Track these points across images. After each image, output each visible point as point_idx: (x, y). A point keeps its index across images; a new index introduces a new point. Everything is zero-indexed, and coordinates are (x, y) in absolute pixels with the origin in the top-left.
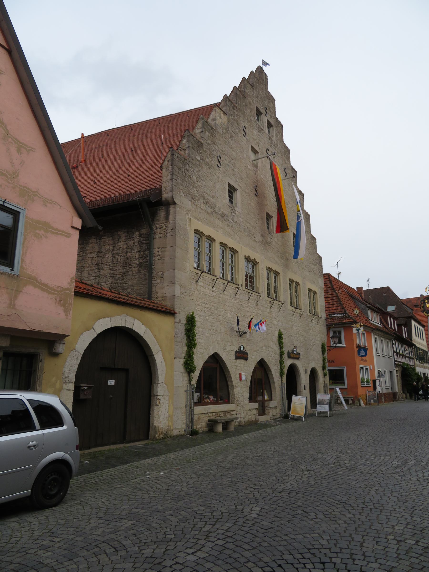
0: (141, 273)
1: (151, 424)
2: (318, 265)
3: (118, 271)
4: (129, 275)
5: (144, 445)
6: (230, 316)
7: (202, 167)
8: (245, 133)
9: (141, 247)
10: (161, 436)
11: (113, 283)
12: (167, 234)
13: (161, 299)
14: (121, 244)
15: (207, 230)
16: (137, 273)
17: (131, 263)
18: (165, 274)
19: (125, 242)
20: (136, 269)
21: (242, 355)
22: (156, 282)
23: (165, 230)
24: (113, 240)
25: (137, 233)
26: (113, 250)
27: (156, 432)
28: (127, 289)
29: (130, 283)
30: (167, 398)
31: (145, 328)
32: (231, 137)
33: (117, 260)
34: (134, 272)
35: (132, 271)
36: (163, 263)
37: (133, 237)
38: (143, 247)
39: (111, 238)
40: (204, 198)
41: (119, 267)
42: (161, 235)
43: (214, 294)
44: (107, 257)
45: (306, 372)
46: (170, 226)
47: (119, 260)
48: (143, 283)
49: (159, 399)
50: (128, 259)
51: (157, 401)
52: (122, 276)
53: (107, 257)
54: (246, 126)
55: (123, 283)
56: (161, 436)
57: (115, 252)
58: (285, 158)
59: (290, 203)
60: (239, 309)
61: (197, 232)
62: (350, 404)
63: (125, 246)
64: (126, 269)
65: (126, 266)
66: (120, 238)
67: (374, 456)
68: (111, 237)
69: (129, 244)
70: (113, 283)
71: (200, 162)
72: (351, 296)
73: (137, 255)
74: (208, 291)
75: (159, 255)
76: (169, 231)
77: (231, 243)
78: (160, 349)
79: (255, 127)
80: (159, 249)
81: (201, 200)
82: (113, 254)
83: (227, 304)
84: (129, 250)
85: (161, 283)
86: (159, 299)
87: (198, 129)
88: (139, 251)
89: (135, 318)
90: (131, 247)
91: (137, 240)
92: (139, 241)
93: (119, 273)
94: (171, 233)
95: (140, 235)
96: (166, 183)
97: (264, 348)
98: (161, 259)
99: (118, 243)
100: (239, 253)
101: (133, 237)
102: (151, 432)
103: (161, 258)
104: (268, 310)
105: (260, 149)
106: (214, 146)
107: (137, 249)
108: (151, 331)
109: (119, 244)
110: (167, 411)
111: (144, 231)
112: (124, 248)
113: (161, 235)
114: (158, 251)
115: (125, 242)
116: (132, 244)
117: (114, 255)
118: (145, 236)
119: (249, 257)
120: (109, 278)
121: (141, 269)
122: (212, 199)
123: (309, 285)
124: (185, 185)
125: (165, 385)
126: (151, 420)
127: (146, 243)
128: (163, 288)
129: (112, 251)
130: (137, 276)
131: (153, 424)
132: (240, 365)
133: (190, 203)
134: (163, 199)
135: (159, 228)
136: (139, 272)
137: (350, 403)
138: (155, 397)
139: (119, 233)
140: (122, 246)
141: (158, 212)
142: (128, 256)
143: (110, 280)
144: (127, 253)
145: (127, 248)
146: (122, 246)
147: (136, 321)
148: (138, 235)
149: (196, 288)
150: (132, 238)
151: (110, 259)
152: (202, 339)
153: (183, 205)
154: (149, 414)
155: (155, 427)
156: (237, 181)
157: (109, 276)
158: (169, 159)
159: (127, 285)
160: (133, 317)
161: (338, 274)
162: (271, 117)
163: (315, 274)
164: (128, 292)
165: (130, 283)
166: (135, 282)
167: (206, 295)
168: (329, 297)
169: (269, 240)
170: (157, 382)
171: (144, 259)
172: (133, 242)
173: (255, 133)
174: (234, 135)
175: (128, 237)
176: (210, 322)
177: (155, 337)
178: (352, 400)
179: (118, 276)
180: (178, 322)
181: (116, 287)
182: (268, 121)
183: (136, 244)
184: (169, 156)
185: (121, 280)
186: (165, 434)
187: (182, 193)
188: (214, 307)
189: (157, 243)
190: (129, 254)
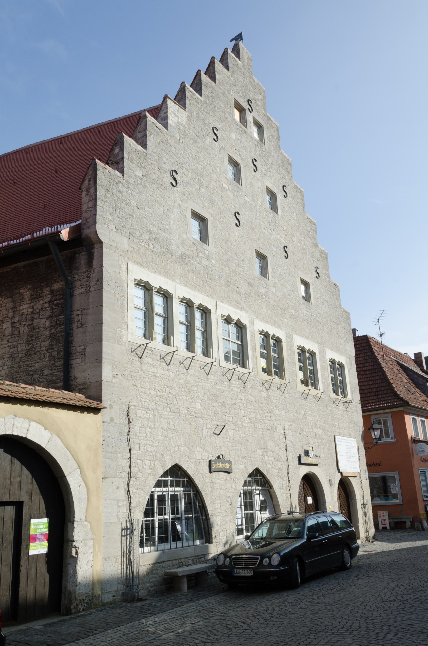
0: (53, 349)
1: (63, 588)
2: (343, 324)
3: (19, 349)
4: (36, 353)
5: (45, 626)
6: (200, 407)
7: (145, 187)
8: (217, 137)
9: (53, 309)
10: (80, 606)
11: (13, 367)
12: (90, 288)
13: (82, 387)
14: (25, 308)
15: (156, 281)
16: (47, 350)
17: (39, 335)
18: (88, 349)
19: (30, 304)
20: (46, 343)
21: (218, 466)
22: (76, 362)
23: (87, 283)
24: (12, 301)
25: (48, 289)
26: (14, 317)
27: (71, 603)
28: (32, 375)
29: (37, 365)
30: (91, 543)
31: (49, 435)
32: (194, 142)
33: (19, 331)
34: (44, 348)
35: (40, 347)
36: (85, 332)
37: (41, 295)
38: (56, 310)
39: (10, 299)
40: (151, 232)
41: (22, 342)
42: (82, 290)
43: (172, 375)
44: (4, 328)
45: (330, 484)
46: (94, 276)
47: (21, 332)
48: (57, 364)
49: (75, 547)
50: (34, 329)
51: (74, 551)
52: (26, 355)
53: (4, 328)
54: (218, 127)
55: (28, 365)
56: (80, 606)
57: (17, 319)
58: (283, 172)
59: (293, 236)
60: (215, 395)
61: (139, 284)
62: (409, 528)
63: (30, 310)
64: (32, 344)
65: (32, 340)
66: (23, 298)
67: (400, 635)
68: (10, 297)
69: (35, 308)
70: (13, 367)
71: (142, 180)
72: (402, 366)
73: (48, 323)
74: (160, 371)
75: (79, 321)
76: (92, 284)
77: (198, 299)
78: (76, 466)
79: (233, 128)
80: (79, 312)
81: (146, 236)
82: (12, 323)
83: (195, 389)
84: (36, 316)
85: (82, 362)
86: (80, 387)
87: (140, 132)
88: (51, 317)
89: (31, 420)
90: (38, 311)
91: (47, 300)
92: (50, 301)
93: (21, 351)
94: (96, 286)
95: (52, 292)
96: (86, 212)
97: (260, 452)
98: (81, 327)
99: (20, 305)
100: (213, 311)
101: (41, 295)
102: (64, 601)
103: (82, 324)
104: (264, 394)
105: (242, 159)
106: (165, 157)
107: (47, 313)
108: (61, 439)
109: (22, 307)
110: (90, 565)
111: (57, 286)
112: (29, 313)
113: (82, 290)
114: (78, 315)
115: (30, 304)
116: (40, 307)
117: (14, 325)
118: (58, 293)
119: (229, 316)
120: (6, 359)
121: (53, 343)
122: (164, 233)
123: (331, 355)
124: (118, 213)
125: (86, 523)
126: (63, 582)
127: (60, 304)
128: (84, 371)
129: (12, 319)
130: (48, 355)
131: (66, 588)
132: (218, 481)
133: (126, 240)
134: (83, 236)
135: (79, 280)
136: (50, 347)
137: (407, 527)
138: (70, 544)
139: (21, 291)
140: (25, 311)
141: (77, 256)
142: (35, 324)
143: (9, 363)
144: (32, 319)
145: (32, 313)
146: (25, 311)
147: (33, 424)
148: (48, 293)
149: (141, 367)
150: (41, 297)
151: (9, 331)
152: (152, 445)
153: (114, 244)
154: (62, 572)
155: (70, 591)
156: (205, 206)
157: (8, 356)
158: (90, 177)
159: (33, 368)
160: (28, 419)
161: (381, 336)
162: (259, 114)
163: (339, 336)
164: (34, 380)
165: (37, 365)
166: (44, 363)
167: (156, 377)
168: (368, 370)
169: (262, 291)
170: (72, 520)
171: (57, 328)
172: (41, 302)
173: (234, 137)
174: (198, 140)
175: (35, 296)
176: (165, 418)
177: (67, 447)
178: (411, 521)
179: (20, 355)
180: (109, 420)
181: (18, 372)
182: (254, 119)
183: (46, 305)
184: (91, 172)
185: (25, 362)
186: (87, 603)
187: (112, 227)
188: (172, 394)
189: (78, 302)
190: (35, 321)
